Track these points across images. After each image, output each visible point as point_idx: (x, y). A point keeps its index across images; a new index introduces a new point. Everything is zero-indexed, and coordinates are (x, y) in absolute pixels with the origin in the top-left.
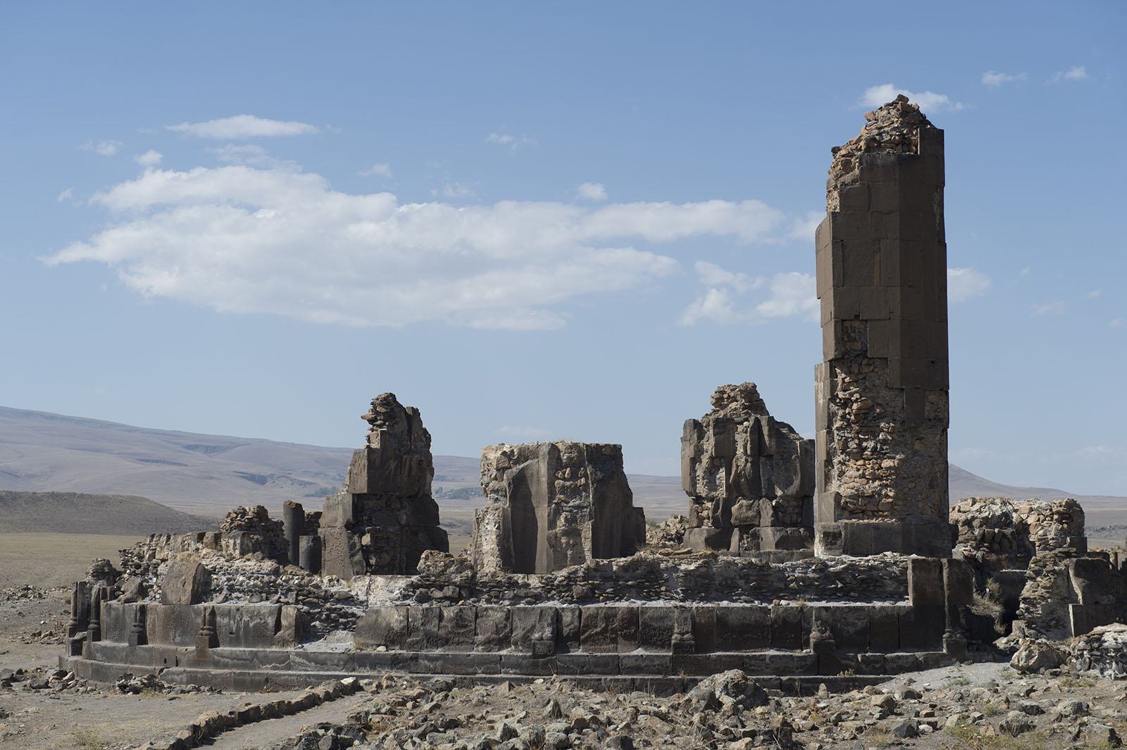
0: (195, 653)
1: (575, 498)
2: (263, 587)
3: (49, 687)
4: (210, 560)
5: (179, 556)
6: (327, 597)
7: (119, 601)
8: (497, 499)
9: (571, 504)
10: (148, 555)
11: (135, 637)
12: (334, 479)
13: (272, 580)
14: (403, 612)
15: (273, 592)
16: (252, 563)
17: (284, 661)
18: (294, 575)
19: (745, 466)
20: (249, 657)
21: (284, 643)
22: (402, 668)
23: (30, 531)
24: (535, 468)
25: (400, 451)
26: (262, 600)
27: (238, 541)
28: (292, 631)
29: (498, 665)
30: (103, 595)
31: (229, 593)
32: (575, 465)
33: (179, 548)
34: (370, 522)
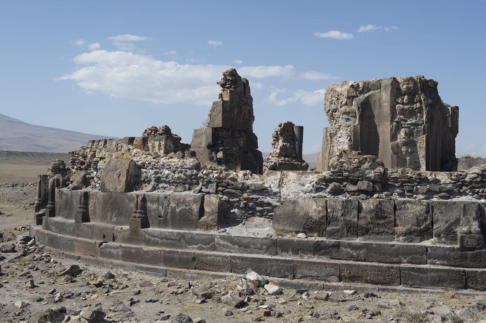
0: (130, 231)
1: (412, 118)
2: (186, 180)
3: (15, 251)
4: (140, 157)
5: (114, 155)
6: (244, 188)
7: (68, 188)
8: (348, 119)
9: (409, 122)
10: (90, 155)
11: (80, 217)
13: (194, 173)
14: (322, 203)
15: (195, 184)
16: (175, 160)
17: (210, 243)
18: (213, 170)
20: (177, 238)
21: (208, 227)
22: (324, 254)
24: (378, 96)
25: (240, 103)
26: (185, 190)
27: (163, 143)
28: (215, 217)
29: (425, 256)
30: (57, 184)
31: (156, 183)
32: (412, 94)
33: (114, 149)
34: (222, 144)
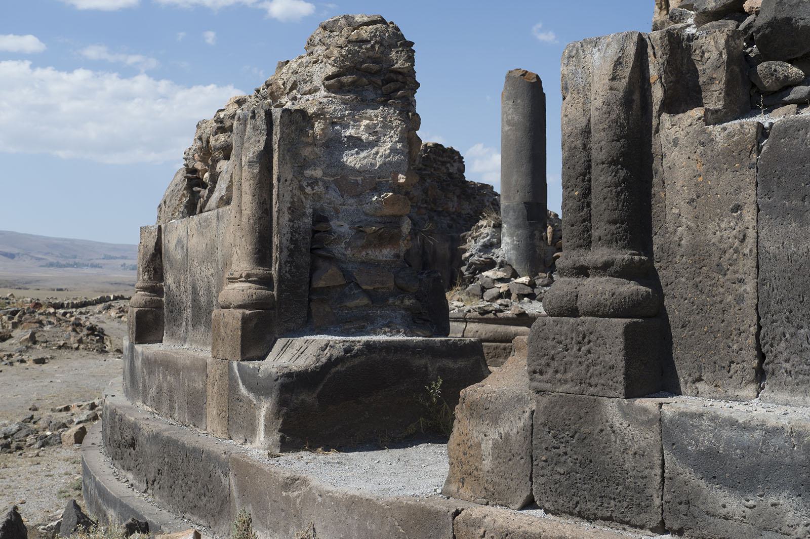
12: (57, 257)
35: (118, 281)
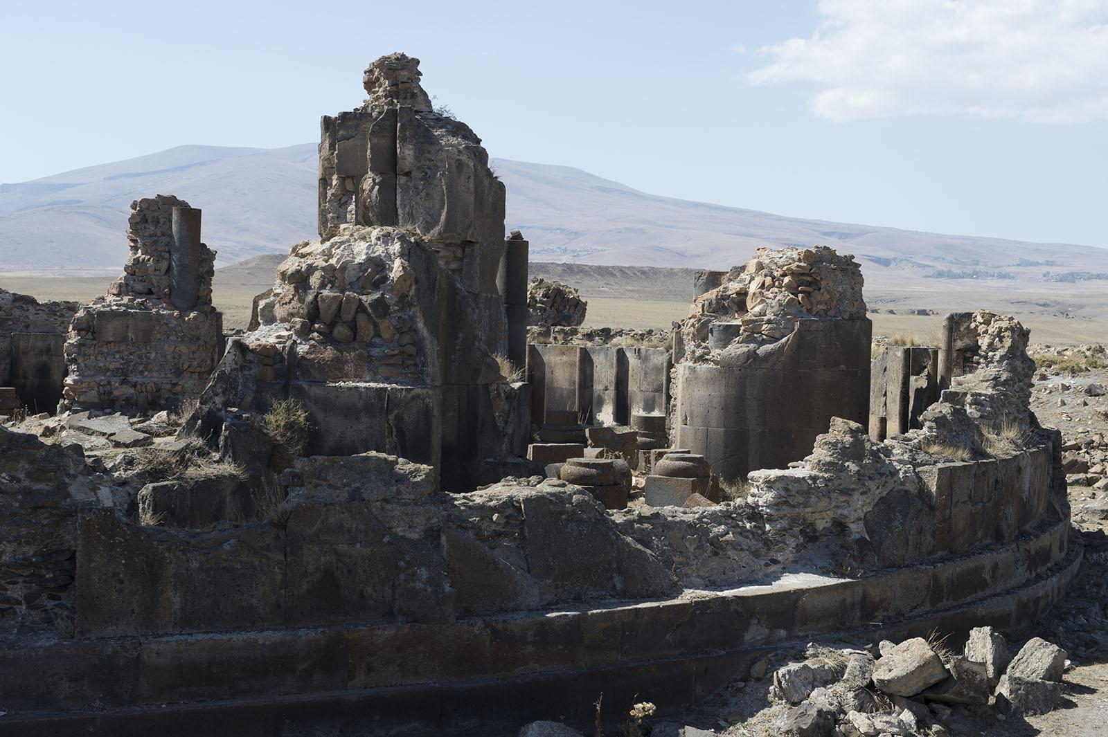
12: (951, 262)
19: (371, 190)
23: (665, 300)
35: (1022, 299)
